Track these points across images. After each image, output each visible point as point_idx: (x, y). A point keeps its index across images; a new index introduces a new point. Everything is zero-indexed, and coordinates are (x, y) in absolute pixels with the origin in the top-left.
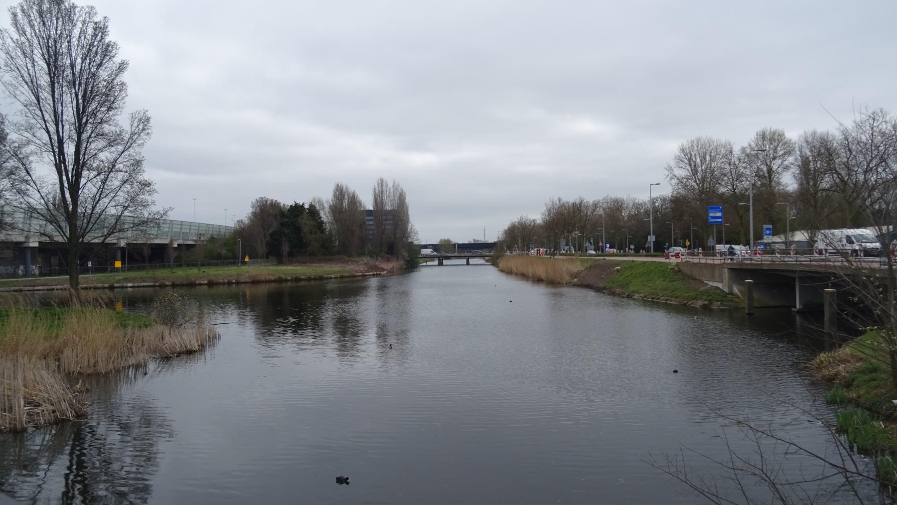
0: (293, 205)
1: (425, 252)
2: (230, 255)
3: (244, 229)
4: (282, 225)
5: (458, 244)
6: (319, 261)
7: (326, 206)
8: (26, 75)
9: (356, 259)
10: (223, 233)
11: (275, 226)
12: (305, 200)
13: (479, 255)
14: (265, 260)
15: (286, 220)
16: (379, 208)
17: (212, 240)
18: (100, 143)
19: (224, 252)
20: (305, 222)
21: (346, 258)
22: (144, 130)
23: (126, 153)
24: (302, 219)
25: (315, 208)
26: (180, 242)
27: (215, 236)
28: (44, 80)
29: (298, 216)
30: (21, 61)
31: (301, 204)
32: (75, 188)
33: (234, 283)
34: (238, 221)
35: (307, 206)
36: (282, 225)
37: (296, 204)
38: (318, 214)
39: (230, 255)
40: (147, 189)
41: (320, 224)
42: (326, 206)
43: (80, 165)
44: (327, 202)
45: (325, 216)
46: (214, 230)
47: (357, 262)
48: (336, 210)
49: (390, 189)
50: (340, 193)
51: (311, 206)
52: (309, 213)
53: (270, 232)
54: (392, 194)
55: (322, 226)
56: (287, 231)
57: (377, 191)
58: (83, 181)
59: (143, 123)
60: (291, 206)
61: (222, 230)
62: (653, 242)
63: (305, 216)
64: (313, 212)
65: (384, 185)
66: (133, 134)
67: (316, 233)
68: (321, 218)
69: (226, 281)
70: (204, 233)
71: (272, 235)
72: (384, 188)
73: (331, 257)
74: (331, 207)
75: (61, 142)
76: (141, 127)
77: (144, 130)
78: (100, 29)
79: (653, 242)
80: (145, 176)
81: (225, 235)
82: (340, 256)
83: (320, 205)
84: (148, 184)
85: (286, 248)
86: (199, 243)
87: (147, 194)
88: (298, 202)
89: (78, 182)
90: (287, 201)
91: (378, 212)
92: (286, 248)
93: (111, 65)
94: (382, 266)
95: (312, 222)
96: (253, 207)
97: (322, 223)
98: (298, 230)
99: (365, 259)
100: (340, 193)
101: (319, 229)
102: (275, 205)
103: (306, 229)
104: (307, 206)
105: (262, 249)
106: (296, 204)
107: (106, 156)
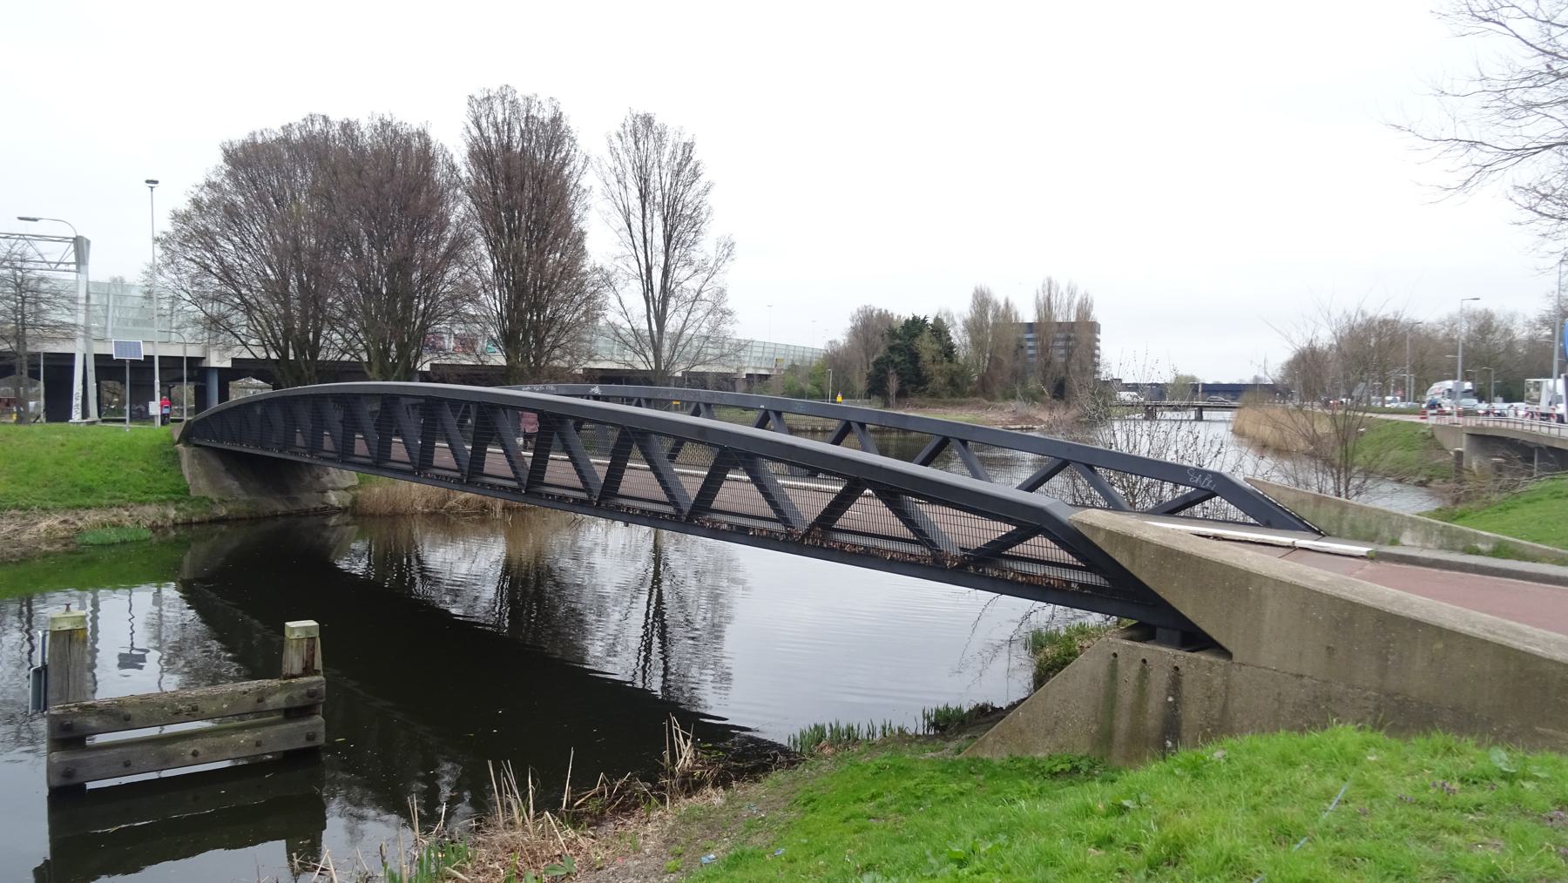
0: (49, 858)
1: (1125, 396)
2: (817, 391)
3: (838, 353)
4: (892, 349)
5: (1204, 385)
6: (945, 404)
7: (959, 321)
8: (620, 202)
9: (1001, 404)
10: (808, 359)
11: (882, 352)
12: (927, 310)
13: (1217, 404)
14: (867, 401)
15: (897, 341)
16: (90, 596)
17: (793, 368)
18: (687, 272)
19: (808, 387)
20: (926, 347)
21: (985, 401)
22: (728, 255)
23: (710, 280)
24: (923, 340)
25: (942, 323)
26: (751, 371)
27: (797, 364)
28: (635, 202)
29: (916, 335)
30: (615, 188)
31: (922, 318)
32: (661, 319)
33: (819, 431)
34: (830, 342)
35: (930, 321)
36: (892, 349)
37: (914, 318)
38: (946, 332)
39: (817, 391)
40: (729, 318)
41: (949, 351)
42: (959, 321)
43: (666, 292)
44: (959, 315)
45: (958, 336)
46: (797, 353)
47: (1001, 408)
48: (975, 327)
49: (1062, 294)
50: (982, 301)
51: (937, 320)
52: (932, 331)
53: (876, 357)
54: (1066, 301)
55: (953, 352)
56: (897, 359)
57: (1041, 297)
58: (669, 311)
59: (728, 248)
60: (907, 321)
61: (807, 354)
62: (154, 400)
63: (926, 335)
64: (939, 330)
65: (1053, 287)
66: (718, 260)
67: (942, 362)
68: (950, 338)
69: (809, 428)
70: (782, 357)
71: (876, 364)
72: (1053, 292)
73: (963, 400)
74: (965, 322)
75: (649, 269)
76: (726, 252)
77: (728, 255)
78: (689, 147)
79: (154, 400)
80: (728, 306)
81: (811, 362)
82: (977, 399)
83: (948, 319)
84: (730, 313)
85: (893, 385)
86: (775, 372)
87: (728, 323)
88: (917, 315)
89: (664, 310)
90: (902, 310)
91: (1043, 328)
92: (893, 385)
93: (699, 186)
94: (1040, 417)
95: (936, 346)
96: (852, 320)
97: (951, 347)
98: (915, 357)
99: (1013, 405)
100: (982, 301)
101: (946, 356)
102: (884, 318)
103: (926, 356)
104: (930, 321)
105: (861, 385)
106: (914, 318)
107: (693, 285)
